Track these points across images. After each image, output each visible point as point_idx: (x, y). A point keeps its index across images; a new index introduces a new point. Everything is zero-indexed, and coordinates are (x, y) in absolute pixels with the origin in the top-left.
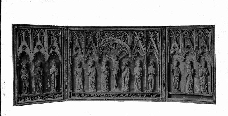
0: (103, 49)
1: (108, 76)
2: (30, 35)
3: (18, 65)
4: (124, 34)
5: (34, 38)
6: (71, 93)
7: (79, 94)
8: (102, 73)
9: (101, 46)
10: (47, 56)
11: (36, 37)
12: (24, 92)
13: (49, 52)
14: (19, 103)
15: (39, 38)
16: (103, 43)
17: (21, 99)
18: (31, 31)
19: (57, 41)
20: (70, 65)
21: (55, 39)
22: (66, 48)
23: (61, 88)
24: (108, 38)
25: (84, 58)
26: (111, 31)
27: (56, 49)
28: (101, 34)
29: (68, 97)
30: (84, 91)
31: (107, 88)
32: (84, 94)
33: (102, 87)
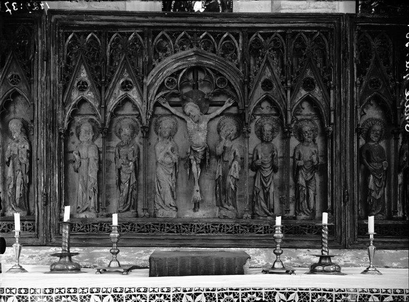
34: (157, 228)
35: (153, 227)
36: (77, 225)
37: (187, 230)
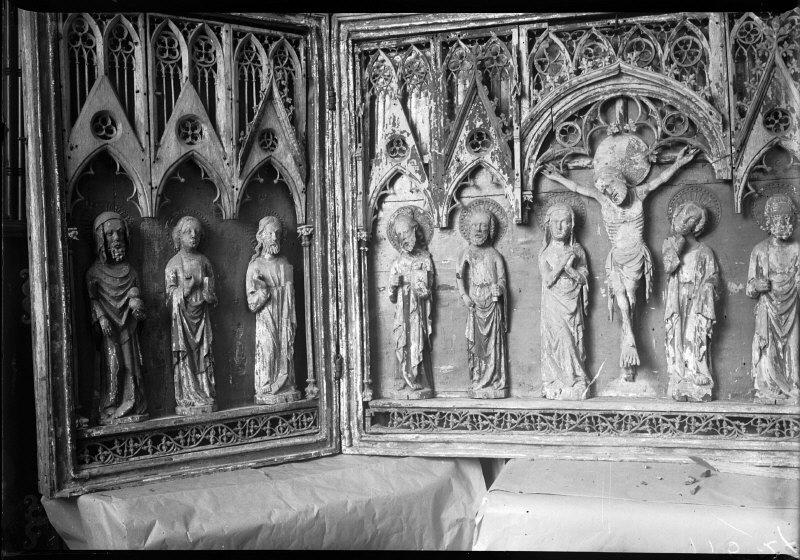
0: (549, 139)
1: (580, 302)
2: (138, 51)
3: (73, 233)
4: (680, 34)
5: (159, 74)
6: (366, 405)
7: (411, 412)
8: (544, 285)
9: (533, 120)
10: (231, 184)
11: (168, 69)
12: (118, 403)
13: (245, 160)
14: (85, 473)
15: (185, 72)
16: (549, 98)
17: (94, 452)
18: (140, 23)
19: (289, 100)
20: (360, 243)
21: (275, 90)
22: (333, 143)
23: (310, 373)
24: (578, 64)
25: (437, 198)
26: (597, 24)
27: (281, 145)
28: (530, 45)
29: (349, 429)
30: (592, 393)
31: (575, 376)
32: (442, 415)
33: (547, 371)
34: (551, 422)
35: (543, 420)
36: (693, 419)
37: (610, 427)
